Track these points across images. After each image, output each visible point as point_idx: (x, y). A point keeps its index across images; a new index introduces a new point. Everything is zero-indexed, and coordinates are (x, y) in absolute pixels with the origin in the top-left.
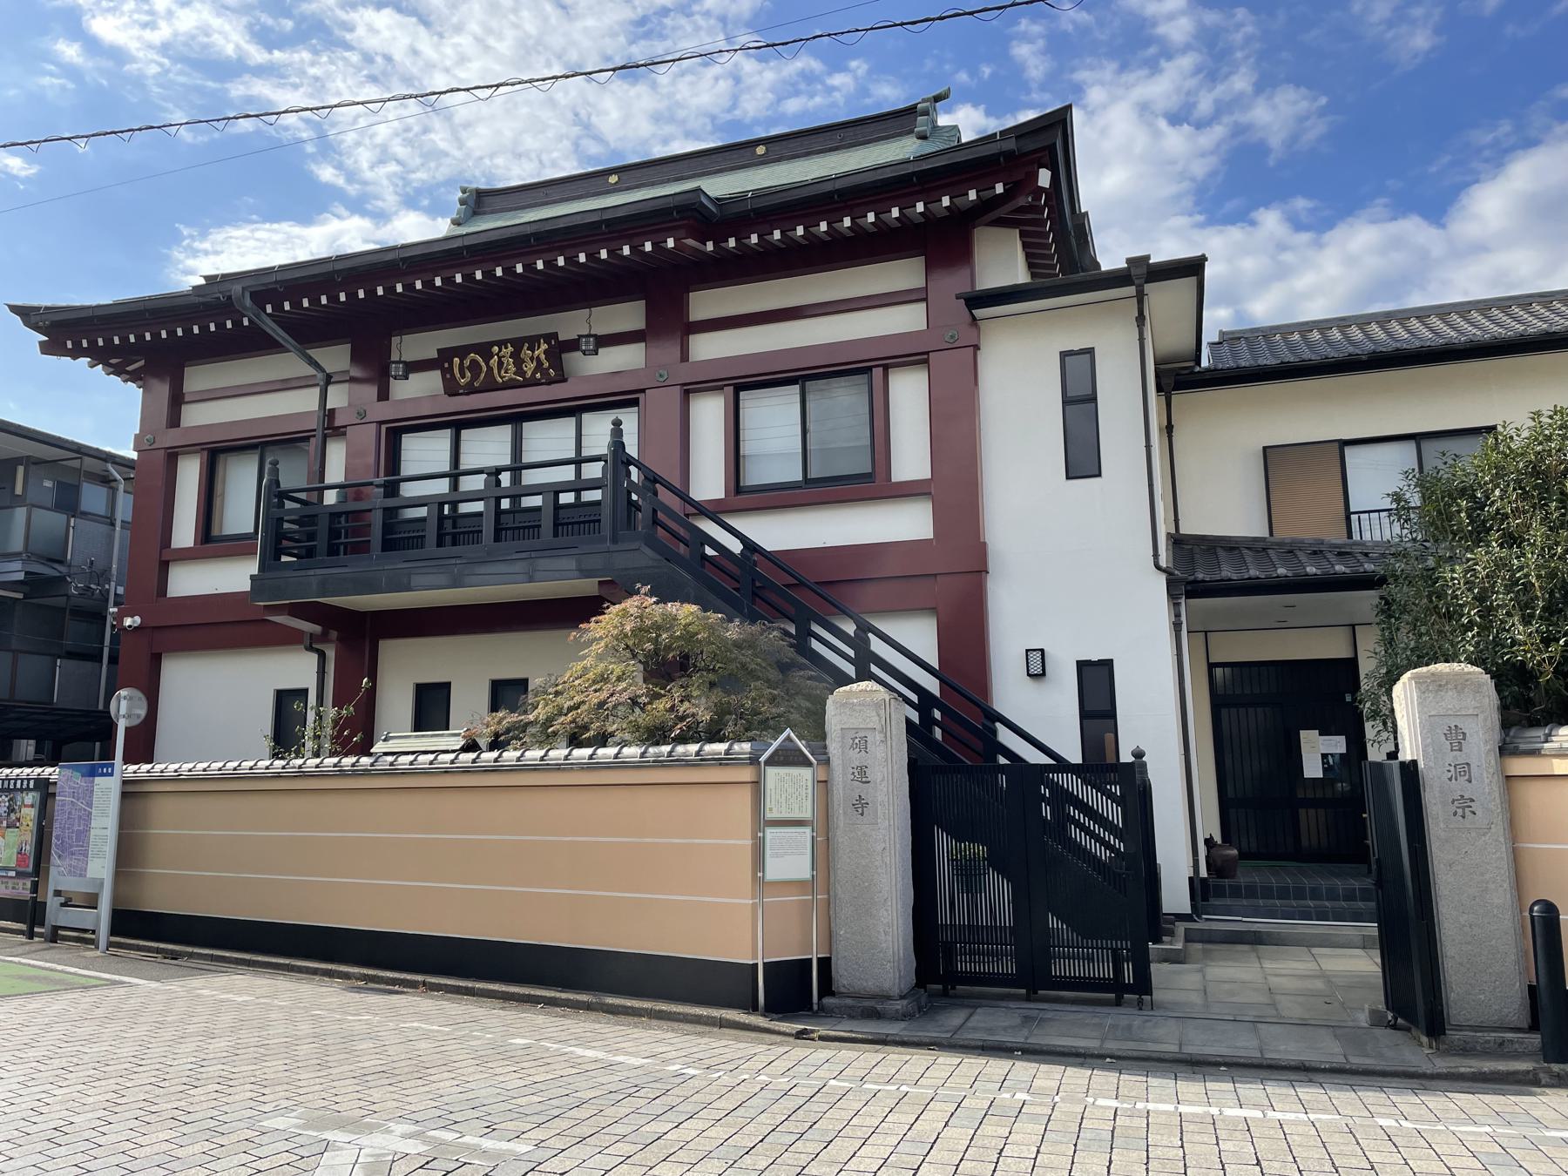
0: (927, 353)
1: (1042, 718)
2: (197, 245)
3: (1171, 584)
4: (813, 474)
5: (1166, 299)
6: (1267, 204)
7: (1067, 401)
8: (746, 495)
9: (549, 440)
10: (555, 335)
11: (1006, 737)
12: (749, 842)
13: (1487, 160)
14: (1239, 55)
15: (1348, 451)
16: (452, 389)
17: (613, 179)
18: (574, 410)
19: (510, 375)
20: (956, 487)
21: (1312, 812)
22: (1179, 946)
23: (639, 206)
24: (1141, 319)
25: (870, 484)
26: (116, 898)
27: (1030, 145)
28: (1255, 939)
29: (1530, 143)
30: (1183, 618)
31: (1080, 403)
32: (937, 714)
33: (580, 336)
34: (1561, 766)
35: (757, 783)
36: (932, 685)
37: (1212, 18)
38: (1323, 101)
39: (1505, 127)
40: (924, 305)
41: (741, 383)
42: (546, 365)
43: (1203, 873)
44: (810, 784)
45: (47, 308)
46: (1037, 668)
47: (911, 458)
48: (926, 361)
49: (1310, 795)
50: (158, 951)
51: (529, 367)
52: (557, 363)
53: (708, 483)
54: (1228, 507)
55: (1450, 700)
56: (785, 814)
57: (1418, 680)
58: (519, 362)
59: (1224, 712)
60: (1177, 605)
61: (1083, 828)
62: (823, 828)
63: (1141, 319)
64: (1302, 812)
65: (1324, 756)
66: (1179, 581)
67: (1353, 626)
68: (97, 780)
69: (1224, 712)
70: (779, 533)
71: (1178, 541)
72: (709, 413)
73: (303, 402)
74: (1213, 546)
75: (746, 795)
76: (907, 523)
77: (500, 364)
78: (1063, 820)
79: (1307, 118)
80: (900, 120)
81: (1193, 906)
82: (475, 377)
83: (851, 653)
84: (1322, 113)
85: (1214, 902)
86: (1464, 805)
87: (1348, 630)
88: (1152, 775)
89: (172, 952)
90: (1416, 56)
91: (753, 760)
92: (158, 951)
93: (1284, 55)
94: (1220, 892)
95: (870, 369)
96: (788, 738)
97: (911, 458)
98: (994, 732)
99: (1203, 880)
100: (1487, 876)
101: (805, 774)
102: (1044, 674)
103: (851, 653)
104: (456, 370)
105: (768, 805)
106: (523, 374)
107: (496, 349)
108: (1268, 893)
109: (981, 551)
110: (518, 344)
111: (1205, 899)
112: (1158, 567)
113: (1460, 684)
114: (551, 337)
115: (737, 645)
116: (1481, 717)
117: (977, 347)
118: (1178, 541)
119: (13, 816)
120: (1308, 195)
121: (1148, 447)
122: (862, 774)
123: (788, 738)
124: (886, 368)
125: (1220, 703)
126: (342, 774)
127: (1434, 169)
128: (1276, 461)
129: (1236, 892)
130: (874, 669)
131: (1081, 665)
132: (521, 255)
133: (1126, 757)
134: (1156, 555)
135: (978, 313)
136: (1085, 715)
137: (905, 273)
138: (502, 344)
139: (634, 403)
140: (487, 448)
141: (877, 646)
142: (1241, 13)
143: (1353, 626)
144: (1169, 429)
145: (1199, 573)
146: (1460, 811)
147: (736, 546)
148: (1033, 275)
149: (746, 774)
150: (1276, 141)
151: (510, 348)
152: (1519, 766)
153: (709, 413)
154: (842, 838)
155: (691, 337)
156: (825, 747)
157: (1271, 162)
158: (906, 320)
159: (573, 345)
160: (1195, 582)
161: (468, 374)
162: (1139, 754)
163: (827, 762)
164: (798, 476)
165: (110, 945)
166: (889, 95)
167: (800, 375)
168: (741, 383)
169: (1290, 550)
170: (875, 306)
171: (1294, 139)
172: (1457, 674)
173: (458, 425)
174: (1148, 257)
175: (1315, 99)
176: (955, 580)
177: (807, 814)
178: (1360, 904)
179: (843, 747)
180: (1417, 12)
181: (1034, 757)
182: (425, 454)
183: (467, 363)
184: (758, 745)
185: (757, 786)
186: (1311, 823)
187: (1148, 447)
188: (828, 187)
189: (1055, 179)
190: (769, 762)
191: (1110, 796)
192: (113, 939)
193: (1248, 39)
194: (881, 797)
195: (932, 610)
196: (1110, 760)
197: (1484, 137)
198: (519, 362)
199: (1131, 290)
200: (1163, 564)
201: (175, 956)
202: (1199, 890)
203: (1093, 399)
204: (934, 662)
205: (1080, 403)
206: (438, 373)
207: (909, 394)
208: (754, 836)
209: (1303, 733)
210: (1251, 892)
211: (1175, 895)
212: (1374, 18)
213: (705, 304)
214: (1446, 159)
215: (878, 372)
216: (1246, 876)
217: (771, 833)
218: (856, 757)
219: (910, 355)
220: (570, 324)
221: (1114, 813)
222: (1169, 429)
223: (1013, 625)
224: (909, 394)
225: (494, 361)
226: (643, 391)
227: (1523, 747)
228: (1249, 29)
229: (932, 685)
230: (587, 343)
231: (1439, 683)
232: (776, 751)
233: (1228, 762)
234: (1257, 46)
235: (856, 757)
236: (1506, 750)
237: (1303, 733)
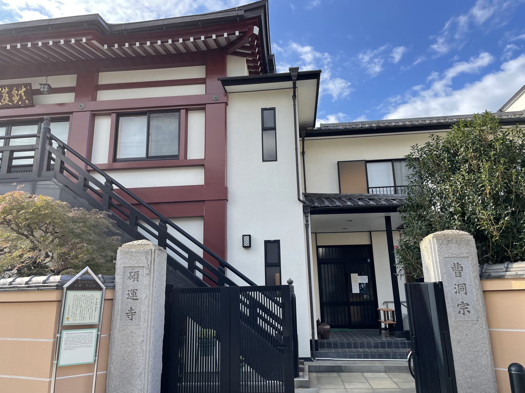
0: (205, 104)
1: (247, 266)
3: (304, 207)
5: (305, 87)
6: (331, 114)
11: (230, 275)
12: (52, 340)
13: (393, 107)
14: (326, 67)
15: (368, 165)
19: (6, 102)
20: (215, 167)
21: (355, 307)
22: (306, 379)
24: (294, 96)
25: (176, 161)
27: (250, 15)
28: (338, 370)
29: (405, 103)
30: (309, 222)
31: (269, 127)
32: (198, 264)
34: (516, 285)
35: (60, 301)
36: (199, 252)
37: (318, 55)
38: (349, 84)
39: (399, 97)
40: (204, 86)
41: (121, 113)
43: (316, 338)
44: (99, 301)
46: (247, 244)
47: (196, 150)
49: (355, 300)
51: (16, 99)
52: (31, 100)
53: (101, 156)
54: (325, 183)
55: (454, 249)
56: (78, 321)
57: (438, 238)
58: (11, 96)
59: (322, 266)
60: (306, 217)
61: (264, 319)
62: (105, 330)
63: (294, 96)
64: (352, 307)
65: (360, 284)
66: (308, 206)
67: (370, 232)
69: (322, 266)
70: (130, 181)
71: (306, 195)
72: (104, 126)
74: (320, 197)
75: (54, 308)
76: (194, 178)
78: (254, 315)
79: (345, 88)
81: (312, 354)
83: (157, 233)
84: (349, 87)
85: (321, 351)
86: (464, 307)
87: (367, 234)
88: (296, 292)
90: (376, 73)
91: (59, 287)
93: (339, 69)
94: (323, 346)
95: (180, 110)
96: (87, 272)
97: (196, 150)
98: (224, 272)
99: (316, 341)
100: (478, 348)
101: (97, 295)
102: (250, 246)
103: (157, 233)
105: (66, 316)
106: (12, 101)
108: (343, 346)
109: (225, 191)
110: (11, 87)
111: (317, 350)
112: (299, 200)
113: (459, 241)
115: (74, 220)
116: (470, 258)
117: (226, 104)
118: (306, 195)
120: (343, 113)
121: (297, 165)
122: (134, 295)
123: (87, 272)
124: (187, 110)
125: (321, 262)
127: (378, 108)
128: (343, 167)
129: (329, 346)
130: (168, 242)
131: (267, 243)
133: (284, 283)
134: (299, 195)
135: (229, 88)
136: (268, 265)
137: (197, 72)
139: (66, 119)
141: (171, 230)
142: (326, 54)
143: (370, 232)
144: (303, 153)
145: (314, 206)
146: (462, 311)
148: (250, 72)
149: (54, 296)
150: (335, 95)
152: (491, 285)
153: (104, 126)
154: (117, 334)
155: (98, 92)
156: (114, 279)
157: (333, 101)
158: (197, 91)
159: (38, 92)
160: (314, 207)
162: (290, 282)
163: (114, 287)
164: (144, 156)
167: (148, 111)
169: (350, 198)
170: (185, 84)
171: (340, 94)
172: (456, 235)
174: (298, 68)
175: (347, 83)
176: (210, 202)
177: (95, 320)
178: (380, 349)
179: (123, 278)
180: (376, 60)
181: (241, 283)
184: (65, 277)
185: (60, 303)
186: (355, 312)
187: (297, 165)
188: (161, 23)
189: (260, 31)
190: (70, 288)
191: (276, 302)
193: (329, 63)
194: (144, 308)
195: (201, 217)
196: (278, 284)
197: (393, 100)
198: (11, 96)
199: (290, 84)
200: (301, 198)
202: (315, 345)
203: (274, 129)
204: (201, 242)
205: (269, 127)
207: (197, 122)
208: (55, 337)
209: (352, 275)
210: (336, 346)
211: (304, 350)
212: (364, 61)
213: (106, 78)
214: (382, 105)
215: (183, 112)
216: (334, 338)
217: (65, 334)
218: (131, 284)
219: (200, 107)
221: (278, 311)
222: (303, 153)
223: (236, 229)
224: (197, 122)
226: (71, 113)
227: (493, 274)
228: (329, 60)
229: (199, 252)
231: (448, 240)
232: (77, 280)
233: (324, 286)
234: (331, 65)
235: (131, 284)
236: (483, 276)
237: (352, 275)
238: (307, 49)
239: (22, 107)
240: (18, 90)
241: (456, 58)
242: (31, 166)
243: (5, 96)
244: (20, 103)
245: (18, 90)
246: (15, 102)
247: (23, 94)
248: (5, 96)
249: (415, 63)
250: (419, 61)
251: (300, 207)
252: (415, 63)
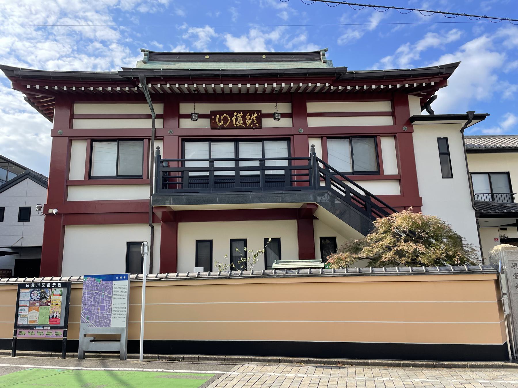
2: (76, 55)
3: (476, 213)
4: (120, 173)
7: (440, 154)
8: (91, 179)
9: (250, 151)
10: (260, 111)
16: (214, 127)
17: (207, 57)
18: (262, 139)
19: (240, 124)
23: (299, 70)
25: (377, 174)
26: (128, 335)
31: (444, 153)
33: (192, 113)
41: (94, 138)
42: (256, 122)
45: (22, 69)
47: (390, 167)
48: (163, 139)
50: (165, 358)
51: (248, 122)
52: (260, 122)
68: (115, 282)
73: (146, 124)
77: (237, 119)
80: (315, 56)
82: (225, 122)
89: (172, 358)
92: (165, 358)
95: (143, 139)
97: (390, 167)
104: (217, 120)
107: (235, 114)
110: (245, 113)
114: (258, 112)
119: (44, 301)
126: (160, 280)
132: (311, 80)
137: (384, 106)
138: (238, 112)
140: (224, 150)
147: (363, 193)
151: (242, 114)
158: (387, 121)
161: (222, 122)
165: (144, 358)
166: (312, 48)
167: (349, 136)
168: (94, 138)
170: (375, 115)
173: (211, 140)
182: (195, 151)
183: (222, 117)
192: (145, 355)
201: (172, 360)
205: (444, 153)
206: (209, 120)
207: (388, 146)
213: (312, 107)
220: (266, 108)
225: (234, 118)
226: (293, 135)
230: (278, 116)
238: (284, 5)
239: (254, 129)
240: (251, 115)
241: (434, 27)
242: (258, 176)
243: (240, 120)
244: (252, 125)
245: (251, 115)
246: (248, 124)
247: (255, 119)
248: (240, 120)
249: (394, 30)
250: (398, 28)
251: (472, 214)
252: (394, 30)
